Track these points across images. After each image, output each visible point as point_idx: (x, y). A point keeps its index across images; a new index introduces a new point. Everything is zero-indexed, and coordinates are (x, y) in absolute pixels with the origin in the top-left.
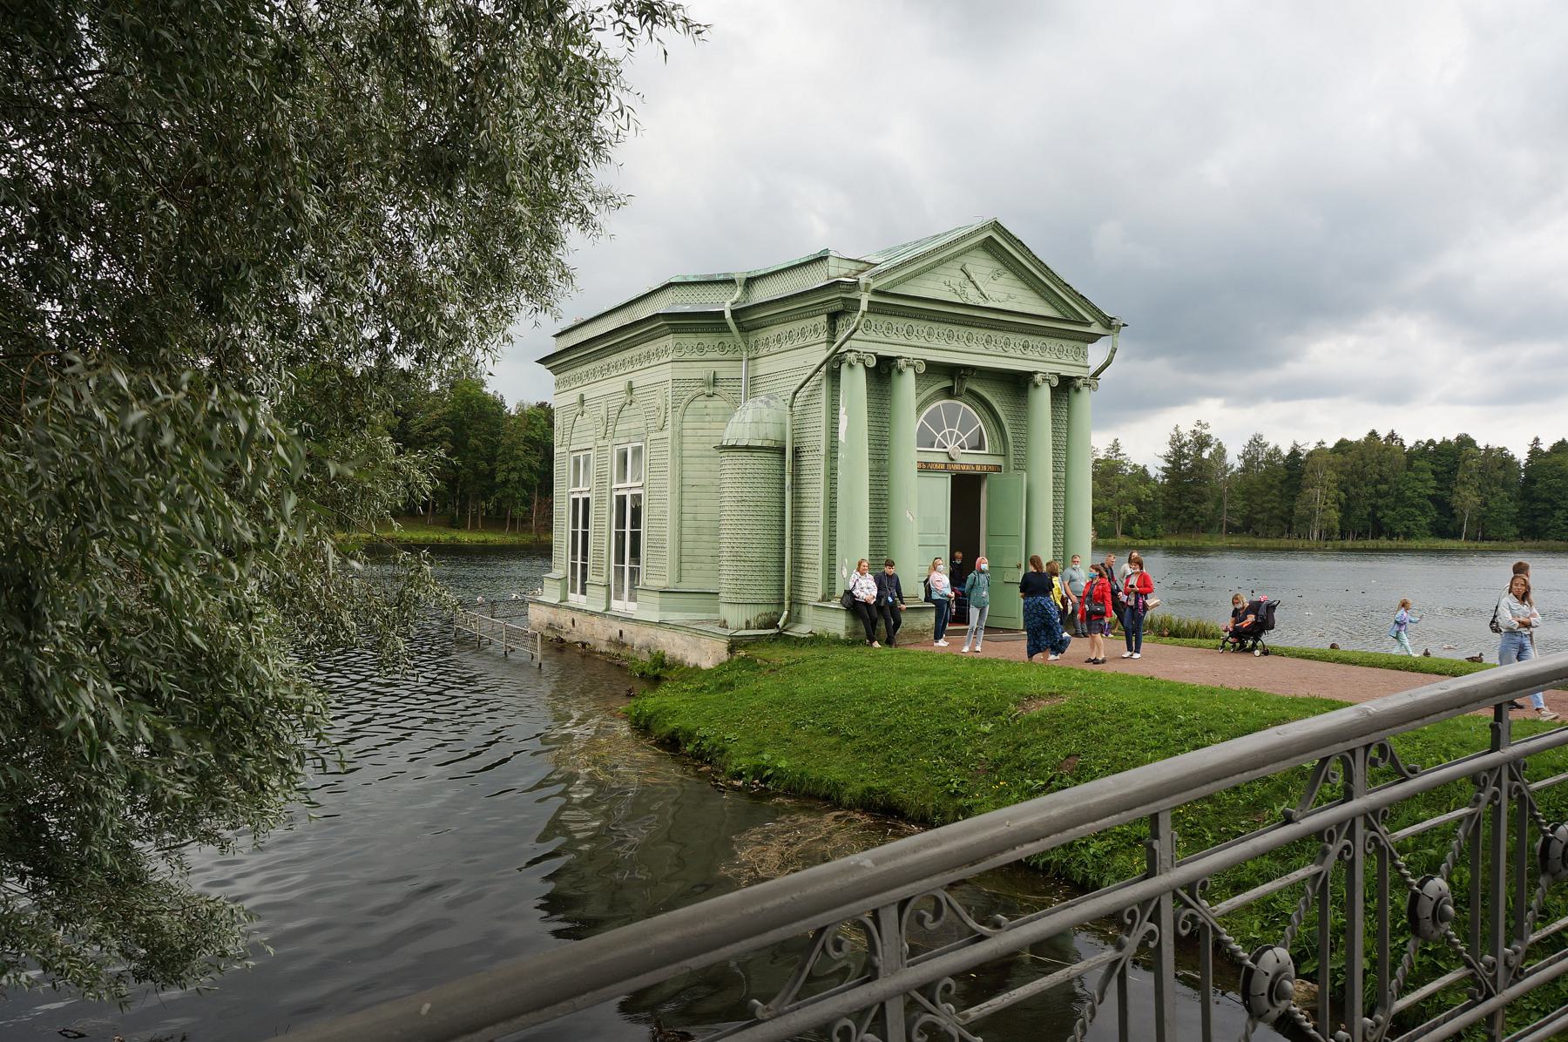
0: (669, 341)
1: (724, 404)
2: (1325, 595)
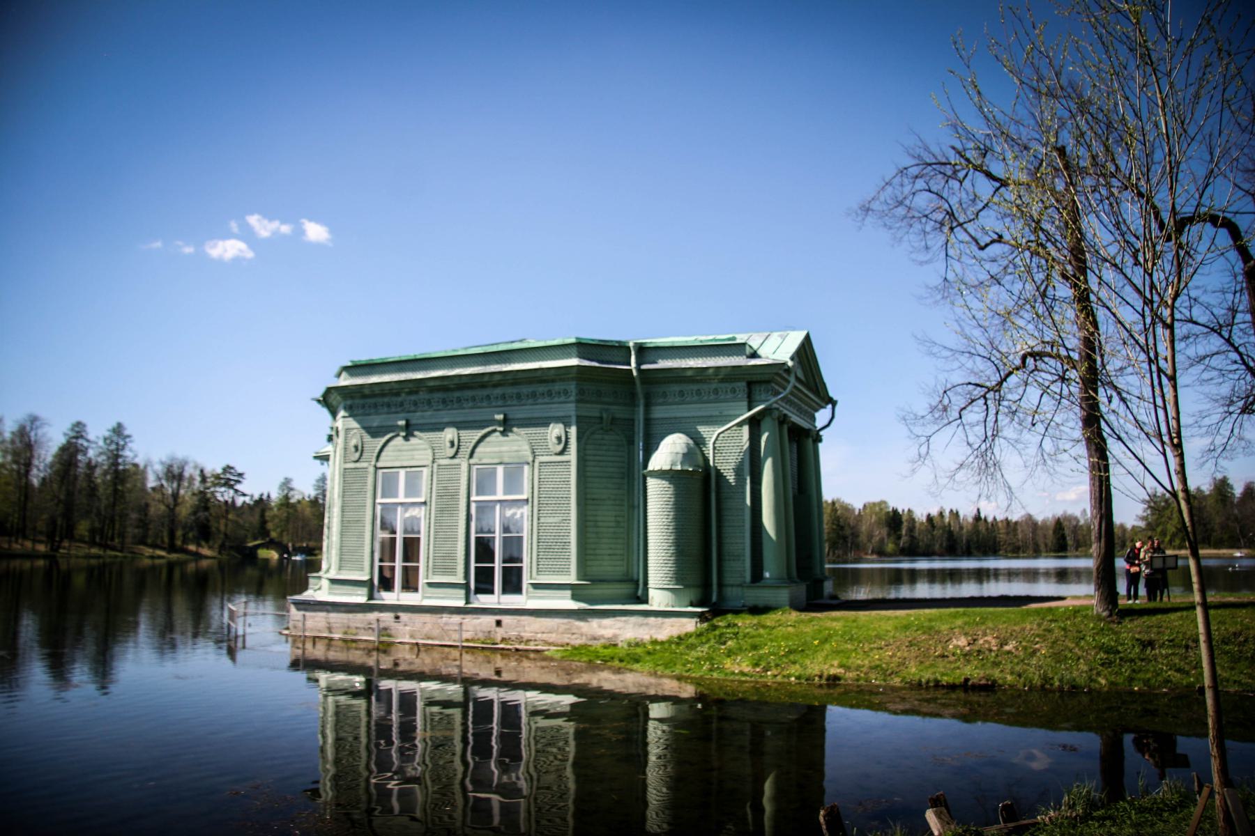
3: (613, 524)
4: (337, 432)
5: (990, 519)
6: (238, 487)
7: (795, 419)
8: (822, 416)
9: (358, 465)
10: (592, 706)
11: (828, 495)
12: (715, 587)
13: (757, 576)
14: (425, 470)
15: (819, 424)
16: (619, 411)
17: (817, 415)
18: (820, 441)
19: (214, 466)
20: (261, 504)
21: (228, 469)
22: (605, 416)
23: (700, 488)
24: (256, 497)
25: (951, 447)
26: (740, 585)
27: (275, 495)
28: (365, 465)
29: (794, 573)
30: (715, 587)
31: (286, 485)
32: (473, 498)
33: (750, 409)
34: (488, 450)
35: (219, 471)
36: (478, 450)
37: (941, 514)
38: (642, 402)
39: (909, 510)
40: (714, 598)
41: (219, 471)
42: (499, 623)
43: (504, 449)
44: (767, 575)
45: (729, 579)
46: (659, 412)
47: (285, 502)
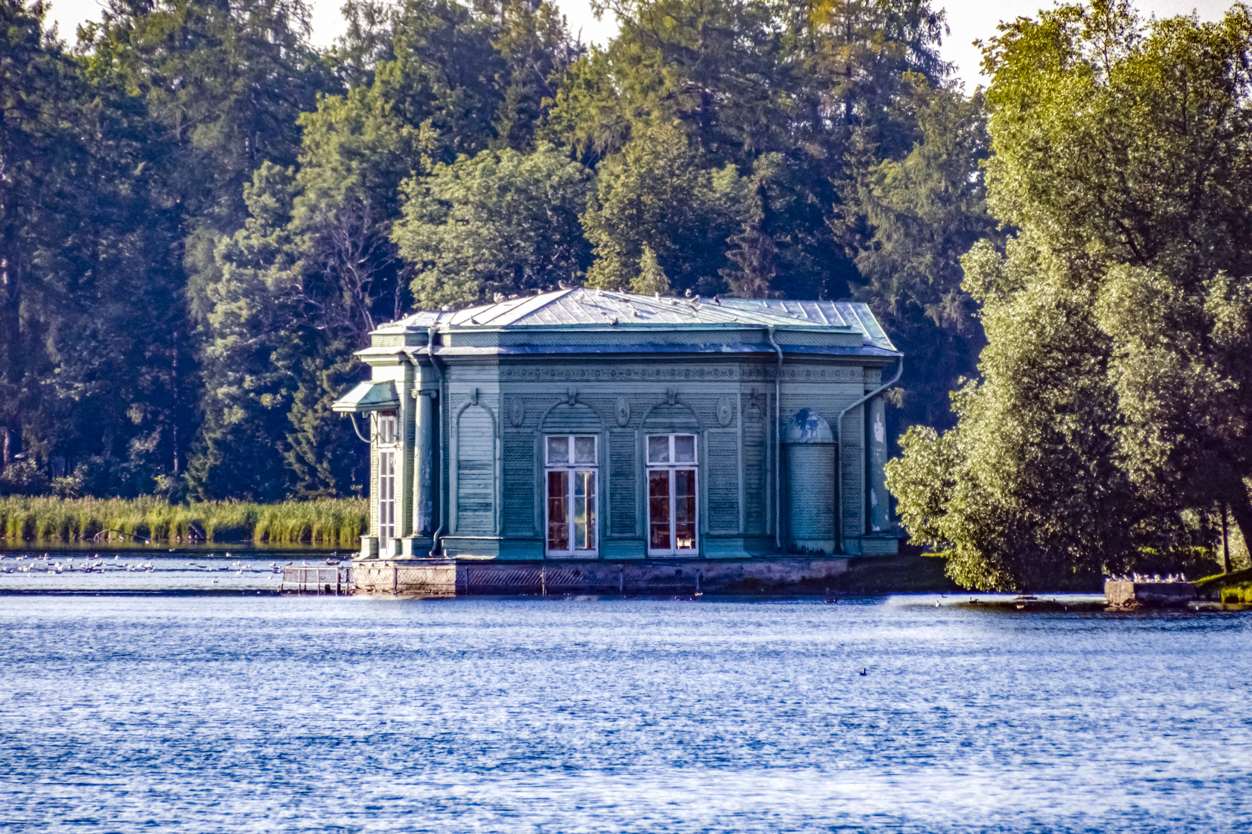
0: (736, 368)
2: (725, 566)
43: (676, 420)
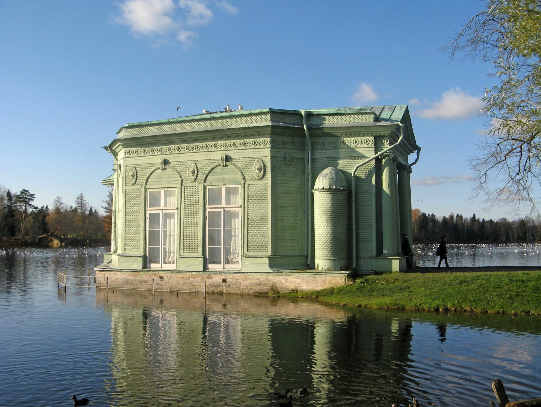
1: (294, 169)
3: (292, 221)
4: (120, 167)
5: (481, 220)
6: (31, 203)
7: (400, 160)
8: (412, 157)
9: (134, 187)
10: (280, 330)
11: (413, 207)
12: (354, 259)
13: (380, 252)
14: (176, 190)
15: (410, 162)
16: (296, 154)
17: (409, 156)
18: (411, 172)
19: (16, 191)
20: (42, 213)
21: (24, 191)
22: (287, 156)
23: (347, 194)
24: (40, 208)
25: (498, 178)
26: (370, 258)
27: (51, 207)
28: (139, 187)
29: (400, 251)
30: (354, 259)
31: (58, 201)
32: (207, 206)
33: (376, 153)
34: (216, 177)
35: (19, 193)
36: (208, 177)
37: (451, 217)
38: (310, 147)
39: (432, 214)
40: (354, 266)
41: (19, 193)
42: (224, 281)
44: (385, 251)
45: (362, 254)
46: (319, 154)
47: (58, 210)
